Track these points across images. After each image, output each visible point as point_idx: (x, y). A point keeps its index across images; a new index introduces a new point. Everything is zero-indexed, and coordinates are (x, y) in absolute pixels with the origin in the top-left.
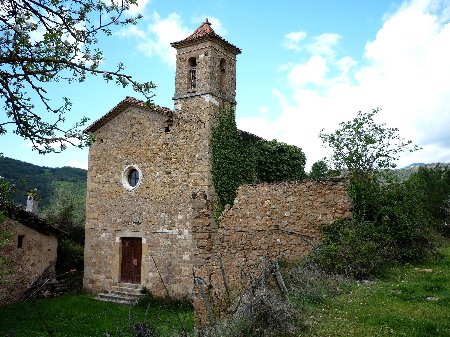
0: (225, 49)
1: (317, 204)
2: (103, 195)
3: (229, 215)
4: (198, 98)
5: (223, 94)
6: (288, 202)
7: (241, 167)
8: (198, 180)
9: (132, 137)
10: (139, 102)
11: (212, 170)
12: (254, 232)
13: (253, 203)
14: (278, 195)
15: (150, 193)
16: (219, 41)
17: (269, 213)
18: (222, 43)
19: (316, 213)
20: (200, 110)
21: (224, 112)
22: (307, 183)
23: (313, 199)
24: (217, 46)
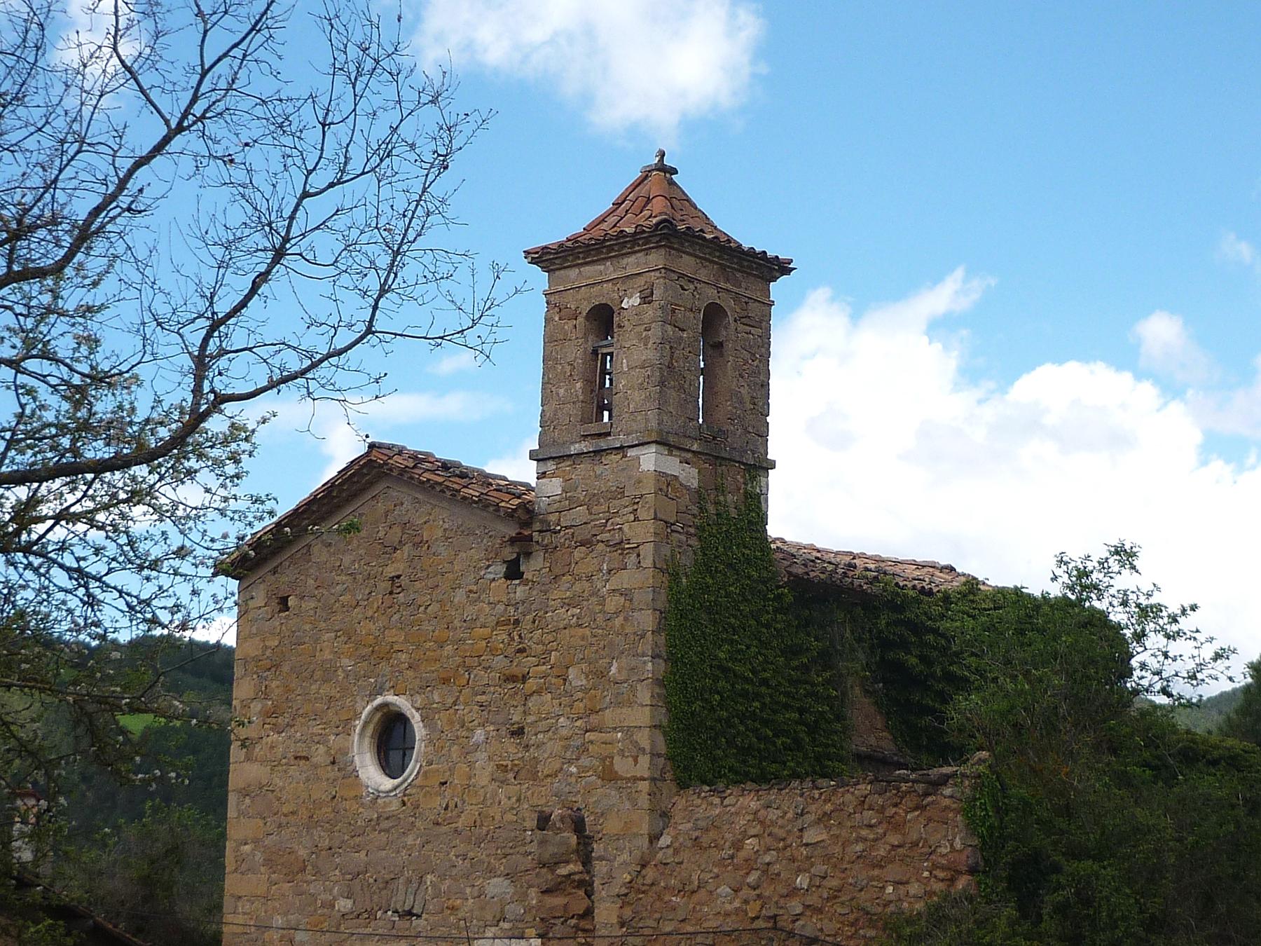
0: (723, 267)
1: (882, 853)
2: (285, 810)
3: (643, 885)
4: (619, 456)
5: (714, 438)
6: (807, 845)
7: (787, 707)
8: (617, 759)
9: (391, 593)
10: (415, 467)
11: (665, 722)
12: (712, 935)
13: (710, 847)
14: (780, 822)
15: (452, 805)
16: (692, 244)
17: (752, 879)
18: (708, 250)
19: (879, 879)
20: (626, 501)
21: (717, 503)
22: (858, 787)
23: (871, 836)
24: (687, 264)
